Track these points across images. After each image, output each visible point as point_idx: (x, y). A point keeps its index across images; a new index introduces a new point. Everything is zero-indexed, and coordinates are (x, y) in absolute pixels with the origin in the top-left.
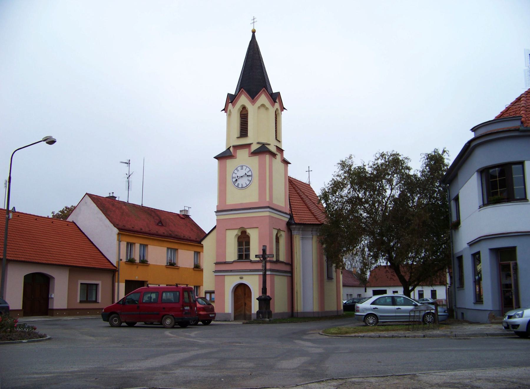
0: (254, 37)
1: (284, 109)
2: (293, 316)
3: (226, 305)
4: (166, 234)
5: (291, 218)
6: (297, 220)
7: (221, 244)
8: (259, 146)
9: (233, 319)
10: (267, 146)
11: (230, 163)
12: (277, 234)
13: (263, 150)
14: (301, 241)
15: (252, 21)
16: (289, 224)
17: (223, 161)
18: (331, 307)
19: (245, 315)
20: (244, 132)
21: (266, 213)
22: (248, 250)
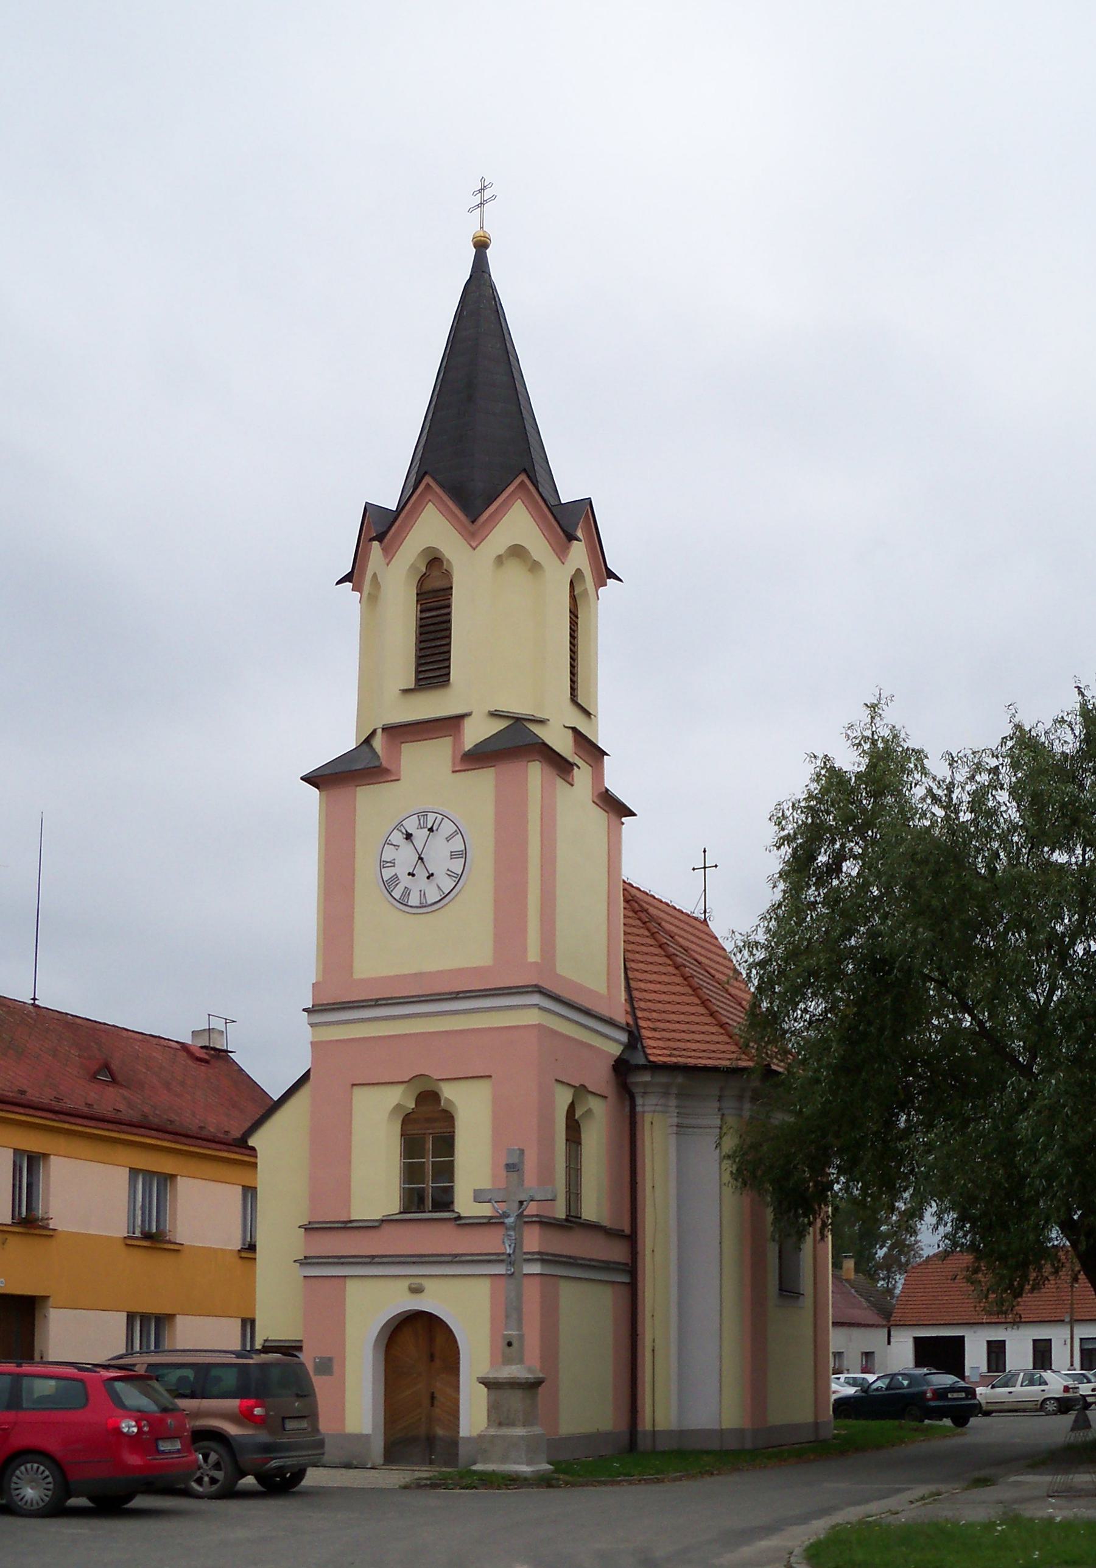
0: (480, 266)
1: (612, 575)
2: (631, 1453)
3: (355, 1401)
4: (128, 1114)
5: (634, 1040)
6: (656, 1050)
7: (331, 1148)
8: (500, 725)
9: (380, 1460)
10: (536, 729)
11: (372, 804)
12: (571, 1109)
13: (516, 744)
14: (673, 1139)
15: (477, 200)
16: (622, 1068)
17: (340, 793)
18: (794, 1409)
19: (430, 1441)
20: (433, 661)
21: (528, 1015)
22: (446, 1171)
